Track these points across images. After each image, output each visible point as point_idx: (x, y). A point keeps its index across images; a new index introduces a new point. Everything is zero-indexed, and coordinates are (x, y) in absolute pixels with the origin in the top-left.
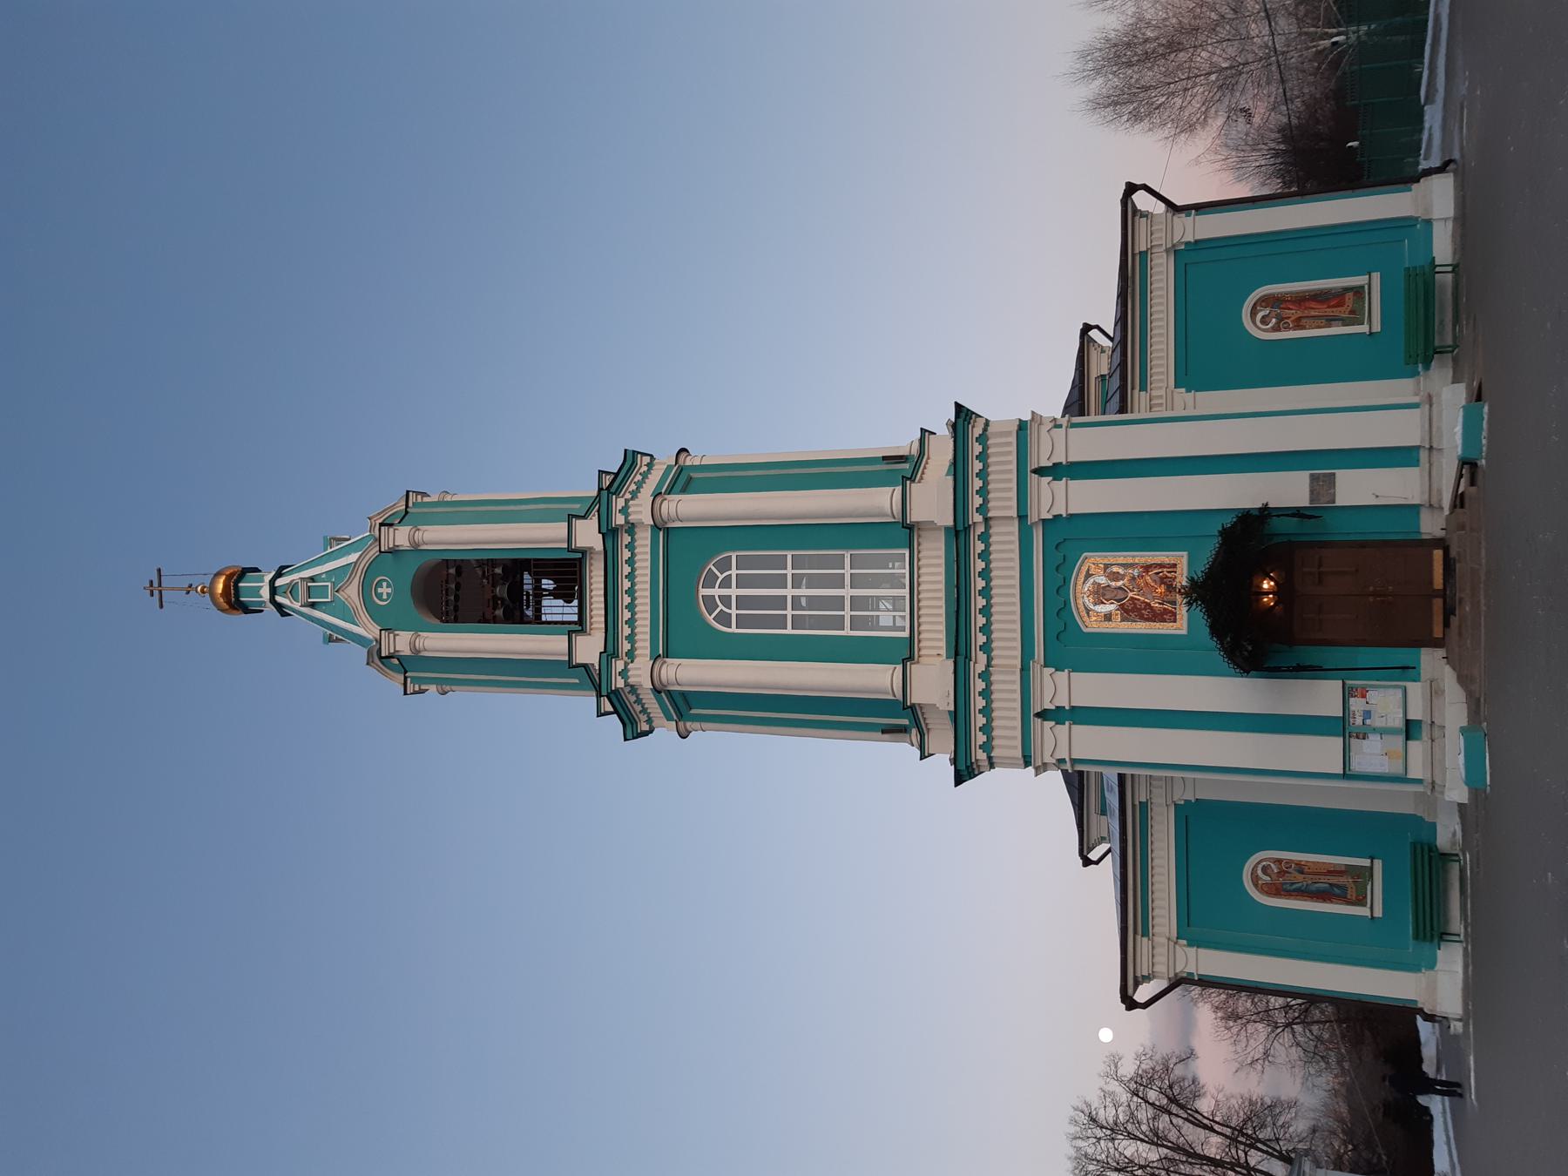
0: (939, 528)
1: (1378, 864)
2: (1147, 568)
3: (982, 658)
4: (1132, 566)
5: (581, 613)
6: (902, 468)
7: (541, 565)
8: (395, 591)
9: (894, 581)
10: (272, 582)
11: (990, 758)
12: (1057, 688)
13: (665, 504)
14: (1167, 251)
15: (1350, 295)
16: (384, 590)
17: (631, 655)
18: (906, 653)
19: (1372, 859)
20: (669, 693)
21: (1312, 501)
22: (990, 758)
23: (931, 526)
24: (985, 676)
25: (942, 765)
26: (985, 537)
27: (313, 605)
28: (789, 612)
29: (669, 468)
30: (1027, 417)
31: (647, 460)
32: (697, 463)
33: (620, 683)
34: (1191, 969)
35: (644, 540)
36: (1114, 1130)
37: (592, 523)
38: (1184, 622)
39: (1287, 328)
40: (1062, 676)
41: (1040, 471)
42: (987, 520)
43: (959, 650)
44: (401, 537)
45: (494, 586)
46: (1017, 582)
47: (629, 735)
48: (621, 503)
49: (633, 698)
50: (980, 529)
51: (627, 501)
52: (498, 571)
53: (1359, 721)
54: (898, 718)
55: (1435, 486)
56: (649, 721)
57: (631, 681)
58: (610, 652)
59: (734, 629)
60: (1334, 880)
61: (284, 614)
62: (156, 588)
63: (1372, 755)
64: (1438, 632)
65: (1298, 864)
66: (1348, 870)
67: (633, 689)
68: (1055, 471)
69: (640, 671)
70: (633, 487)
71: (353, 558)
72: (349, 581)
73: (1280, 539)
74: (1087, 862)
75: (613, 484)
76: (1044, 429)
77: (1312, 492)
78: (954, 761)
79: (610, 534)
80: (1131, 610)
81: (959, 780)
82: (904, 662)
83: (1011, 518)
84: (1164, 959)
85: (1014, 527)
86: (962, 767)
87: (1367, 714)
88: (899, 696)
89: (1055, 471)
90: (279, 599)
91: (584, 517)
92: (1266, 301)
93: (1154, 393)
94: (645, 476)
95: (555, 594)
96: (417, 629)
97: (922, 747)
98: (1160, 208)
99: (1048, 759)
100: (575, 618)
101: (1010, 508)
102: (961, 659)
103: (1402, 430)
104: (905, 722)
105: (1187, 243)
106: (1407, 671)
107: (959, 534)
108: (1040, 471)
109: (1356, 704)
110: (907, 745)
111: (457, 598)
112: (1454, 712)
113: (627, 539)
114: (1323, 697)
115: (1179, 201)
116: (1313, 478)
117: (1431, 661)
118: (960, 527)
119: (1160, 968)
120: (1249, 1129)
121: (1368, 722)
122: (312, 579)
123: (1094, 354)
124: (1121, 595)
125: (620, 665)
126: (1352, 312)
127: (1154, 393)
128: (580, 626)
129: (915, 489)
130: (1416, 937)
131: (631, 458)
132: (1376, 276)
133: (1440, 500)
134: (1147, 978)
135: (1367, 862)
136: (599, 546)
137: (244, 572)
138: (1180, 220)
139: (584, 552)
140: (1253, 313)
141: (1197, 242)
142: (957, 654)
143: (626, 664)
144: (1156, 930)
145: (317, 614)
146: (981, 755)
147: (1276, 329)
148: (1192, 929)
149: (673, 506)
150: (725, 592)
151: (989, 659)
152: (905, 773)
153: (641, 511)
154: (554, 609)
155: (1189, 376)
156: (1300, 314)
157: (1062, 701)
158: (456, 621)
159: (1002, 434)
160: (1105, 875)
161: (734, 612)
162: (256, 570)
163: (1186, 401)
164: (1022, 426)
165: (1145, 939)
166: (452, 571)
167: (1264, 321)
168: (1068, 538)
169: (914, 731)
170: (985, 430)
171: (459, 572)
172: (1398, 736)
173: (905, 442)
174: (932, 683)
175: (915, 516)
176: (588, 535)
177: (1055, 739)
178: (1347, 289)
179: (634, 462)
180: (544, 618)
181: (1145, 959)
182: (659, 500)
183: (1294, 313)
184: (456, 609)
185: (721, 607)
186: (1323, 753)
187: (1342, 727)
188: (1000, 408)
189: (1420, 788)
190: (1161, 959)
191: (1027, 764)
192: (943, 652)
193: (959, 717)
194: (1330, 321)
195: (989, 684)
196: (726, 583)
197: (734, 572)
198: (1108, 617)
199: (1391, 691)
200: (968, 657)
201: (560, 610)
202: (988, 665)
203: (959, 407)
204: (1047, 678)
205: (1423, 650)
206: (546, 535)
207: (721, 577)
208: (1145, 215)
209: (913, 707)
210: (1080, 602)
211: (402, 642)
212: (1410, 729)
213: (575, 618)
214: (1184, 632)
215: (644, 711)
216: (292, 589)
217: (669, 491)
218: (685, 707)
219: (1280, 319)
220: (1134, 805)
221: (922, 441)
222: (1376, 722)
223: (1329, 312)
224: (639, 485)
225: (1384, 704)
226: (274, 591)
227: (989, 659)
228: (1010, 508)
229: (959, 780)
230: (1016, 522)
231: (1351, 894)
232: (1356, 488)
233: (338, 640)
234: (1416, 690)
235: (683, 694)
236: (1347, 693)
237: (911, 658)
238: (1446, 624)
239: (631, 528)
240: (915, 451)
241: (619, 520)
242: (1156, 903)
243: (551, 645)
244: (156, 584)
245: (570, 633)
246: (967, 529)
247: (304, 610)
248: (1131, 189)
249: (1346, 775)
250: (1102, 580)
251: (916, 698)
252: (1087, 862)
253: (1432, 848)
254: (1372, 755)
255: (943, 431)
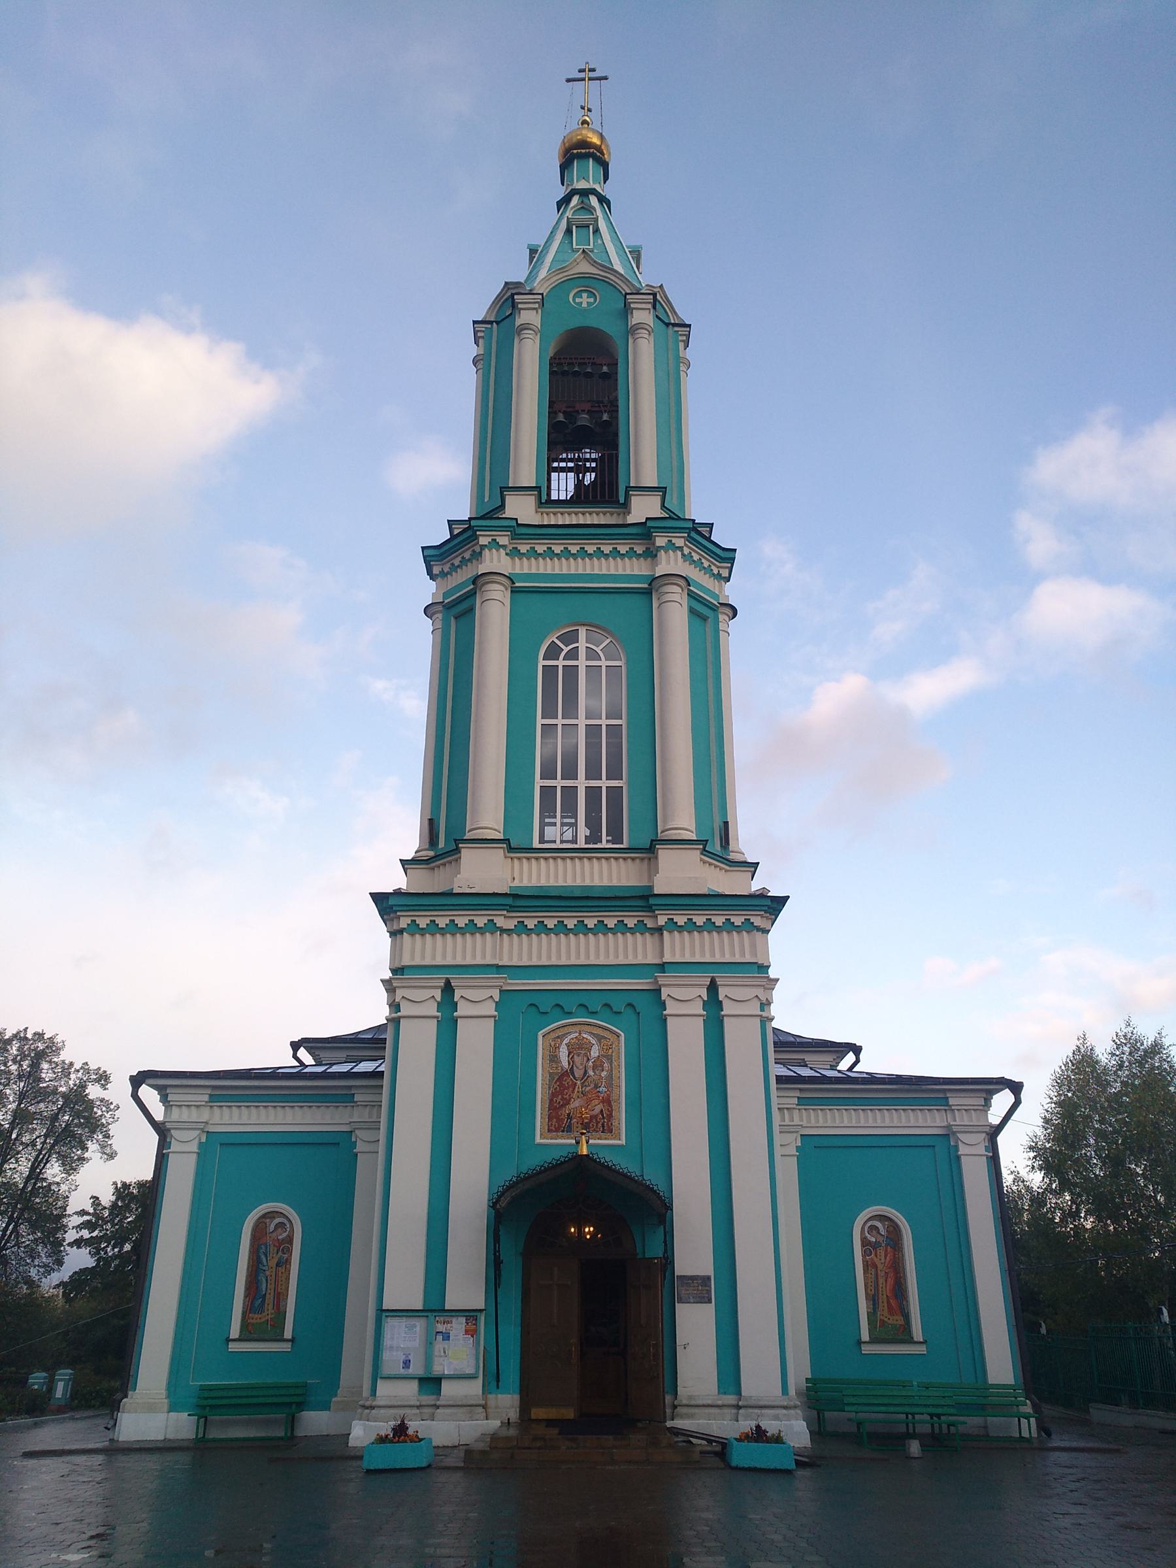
0: (650, 878)
1: (287, 1347)
2: (607, 1101)
3: (511, 924)
4: (609, 1085)
5: (559, 502)
6: (716, 843)
7: (609, 468)
8: (585, 310)
9: (594, 837)
10: (593, 192)
11: (401, 931)
12: (478, 1005)
13: (678, 590)
14: (949, 1127)
15: (900, 1321)
16: (585, 300)
17: (514, 553)
18: (513, 847)
19: (292, 1340)
20: (472, 594)
21: (681, 1277)
22: (401, 931)
23: (653, 870)
24: (492, 928)
25: (396, 880)
26: (641, 928)
27: (569, 231)
28: (560, 721)
29: (716, 597)
30: (772, 973)
31: (725, 573)
32: (722, 626)
33: (483, 541)
34: (175, 1146)
35: (637, 568)
36: (33, 1075)
37: (657, 512)
38: (549, 1144)
39: (865, 1254)
40: (490, 1009)
41: (713, 988)
42: (659, 930)
43: (517, 901)
44: (642, 316)
45: (589, 412)
46: (593, 961)
47: (427, 552)
48: (679, 542)
49: (467, 555)
50: (650, 923)
51: (681, 549)
52: (605, 417)
53: (441, 1327)
54: (443, 839)
55: (696, 1410)
56: (444, 575)
57: (486, 552)
58: (518, 531)
59: (542, 663)
60: (270, 1299)
61: (560, 204)
62: (588, 75)
63: (403, 1339)
64: (538, 1413)
65: (288, 1262)
66: (282, 1315)
67: (477, 556)
68: (713, 1002)
69: (495, 561)
70: (696, 557)
71: (618, 267)
72: (594, 263)
73: (638, 1240)
74: (295, 1046)
75: (699, 534)
76: (760, 992)
77: (693, 1278)
78: (398, 893)
79: (645, 531)
80: (562, 1083)
81: (378, 898)
82: (506, 841)
83: (662, 955)
84: (185, 1118)
85: (652, 959)
86: (392, 901)
87: (446, 1337)
88: (468, 836)
89: (713, 1002)
90: (575, 200)
91: (663, 506)
92: (894, 1233)
93: (796, 1113)
94: (707, 571)
95: (579, 485)
96: (543, 333)
97: (414, 861)
98: (994, 1118)
99: (399, 993)
100: (554, 496)
101: (673, 953)
102: (509, 901)
103: (761, 1375)
104: (441, 844)
105: (957, 1147)
106: (494, 1379)
107: (644, 900)
108: (713, 988)
109: (458, 1326)
110: (416, 846)
111: (576, 374)
112: (444, 1430)
113: (639, 550)
114: (466, 1288)
115: (1001, 1139)
116: (709, 1278)
117: (507, 1403)
118: (652, 901)
119: (176, 1114)
120: (38, 1210)
121: (440, 1337)
122: (597, 231)
123: (829, 1058)
124: (578, 1073)
125: (503, 540)
126: (883, 1322)
127: (796, 1113)
128: (546, 502)
129: (695, 855)
130: (203, 1388)
131: (727, 557)
132: (922, 1349)
133: (682, 1417)
134: (164, 1099)
135: (288, 1334)
136: (631, 519)
137: (605, 165)
138: (981, 1138)
139: (626, 506)
140: (882, 1218)
141: (958, 1158)
142: (515, 896)
143: (504, 547)
144: (217, 1111)
145: (559, 236)
146: (404, 923)
147: (865, 1242)
148: (217, 1146)
149: (676, 597)
150: (582, 653)
151: (508, 932)
152: (387, 838)
153: (669, 563)
154: (563, 486)
155: (816, 1151)
156: (880, 1267)
157: (463, 1009)
158: (552, 373)
159: (753, 946)
160: (283, 1059)
161: (560, 663)
162: (606, 178)
163: (787, 1145)
164: (764, 968)
165: (206, 1098)
166: (605, 369)
167: (873, 1228)
168: (645, 1010)
169: (432, 853)
170: (758, 929)
171: (605, 376)
172: (427, 1370)
173: (746, 843)
174: (482, 871)
175: (665, 856)
176: (643, 508)
177: (424, 1000)
178: (907, 1317)
179: (723, 560)
180: (554, 475)
181: (190, 1097)
182: (682, 583)
183: (881, 1259)
184: (565, 373)
185: (566, 649)
186: (405, 1286)
187: (434, 1309)
188: (783, 946)
189: (366, 1392)
190: (183, 1115)
191: (394, 971)
192: (516, 883)
193: (448, 900)
194: (873, 1299)
195: (482, 931)
196: (591, 654)
197: (604, 663)
198: (554, 1058)
199: (473, 1362)
200: (511, 908)
201: (563, 487)
202: (503, 931)
203: (782, 901)
204: (487, 993)
205: (517, 1397)
206: (643, 462)
207: (598, 650)
208: (987, 1104)
209: (457, 850)
210: (570, 1029)
211: (529, 317)
212: (431, 1383)
213: (554, 496)
214: (623, 1142)
215: (455, 568)
216: (586, 208)
217: (691, 595)
218: (455, 614)
219: (875, 1246)
220: (350, 1087)
221: (745, 864)
222: (440, 1344)
223: (883, 1299)
224: (697, 564)
225: (459, 1354)
226: (585, 193)
227: (508, 932)
228: (673, 953)
229: (378, 898)
230: (657, 961)
231: (255, 1318)
232: (695, 1325)
233: (531, 262)
234: (475, 1389)
235: (472, 609)
236: (470, 1315)
237: (511, 849)
238: (550, 1423)
239: (651, 554)
240: (732, 856)
241: (660, 541)
242: (253, 1110)
243: (526, 464)
244: (592, 75)
245: (537, 488)
246: (650, 909)
247: (564, 221)
248: (1016, 1088)
249: (381, 1311)
250: (595, 1052)
251: (468, 855)
252: (295, 1046)
253: (301, 1406)
254: (403, 1339)
255: (755, 886)
